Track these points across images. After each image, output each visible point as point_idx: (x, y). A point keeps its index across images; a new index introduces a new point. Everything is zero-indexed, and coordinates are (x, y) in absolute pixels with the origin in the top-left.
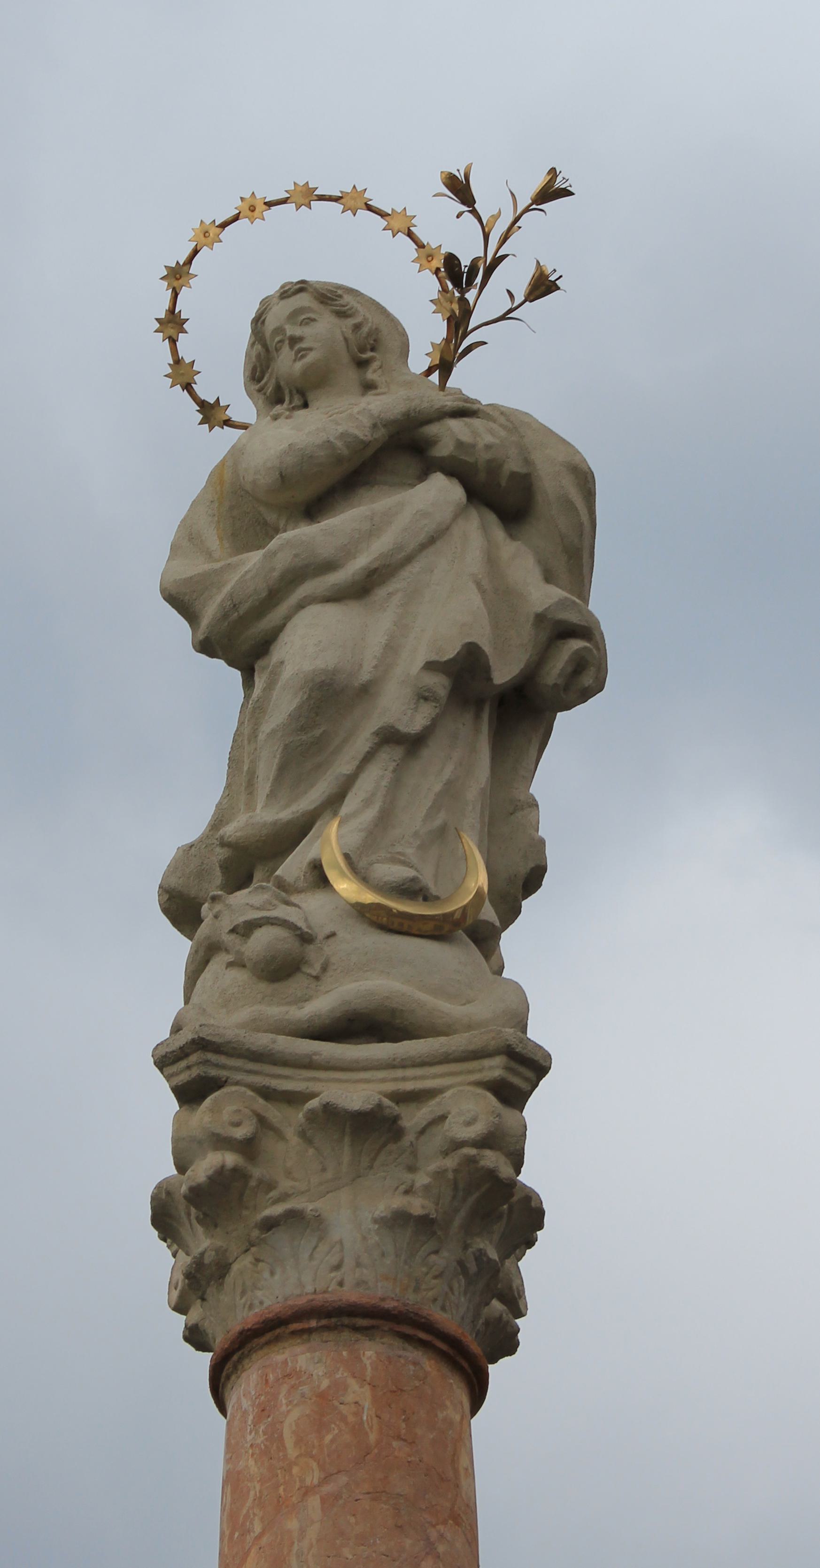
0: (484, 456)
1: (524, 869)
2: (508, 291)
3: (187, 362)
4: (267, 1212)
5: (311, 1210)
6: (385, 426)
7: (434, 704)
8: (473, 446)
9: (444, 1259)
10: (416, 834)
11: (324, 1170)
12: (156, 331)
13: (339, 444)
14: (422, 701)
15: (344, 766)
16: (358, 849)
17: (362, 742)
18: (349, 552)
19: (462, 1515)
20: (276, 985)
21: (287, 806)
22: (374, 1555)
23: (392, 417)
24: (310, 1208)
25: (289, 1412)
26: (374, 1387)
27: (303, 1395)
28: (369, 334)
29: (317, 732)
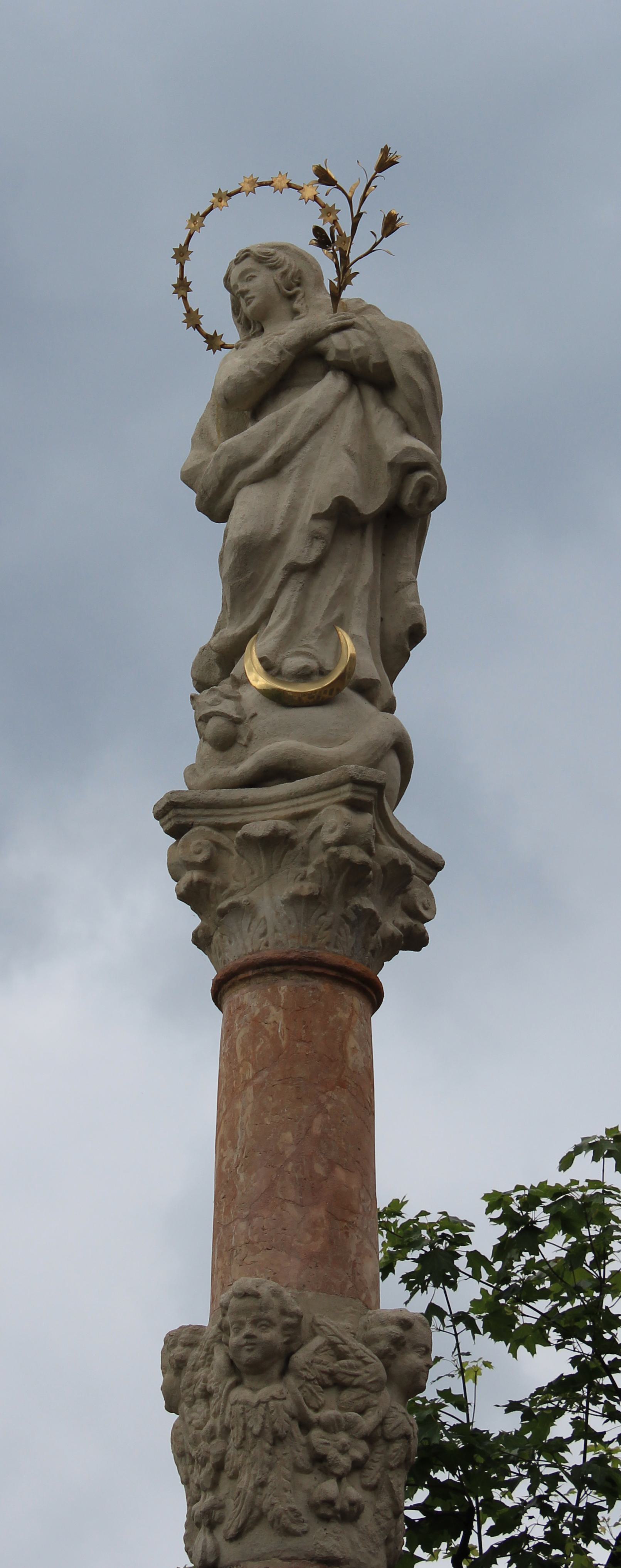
0: (355, 357)
1: (404, 628)
2: (372, 232)
3: (194, 310)
4: (220, 906)
5: (244, 901)
6: (289, 350)
7: (322, 541)
8: (348, 351)
10: (317, 629)
11: (253, 873)
12: (174, 293)
13: (257, 371)
14: (315, 539)
16: (274, 651)
17: (277, 577)
18: (262, 448)
19: (348, 1080)
20: (225, 753)
21: (240, 623)
22: (283, 1120)
23: (294, 343)
24: (244, 900)
25: (239, 1031)
26: (285, 1009)
27: (246, 1021)
28: (293, 277)
29: (248, 575)
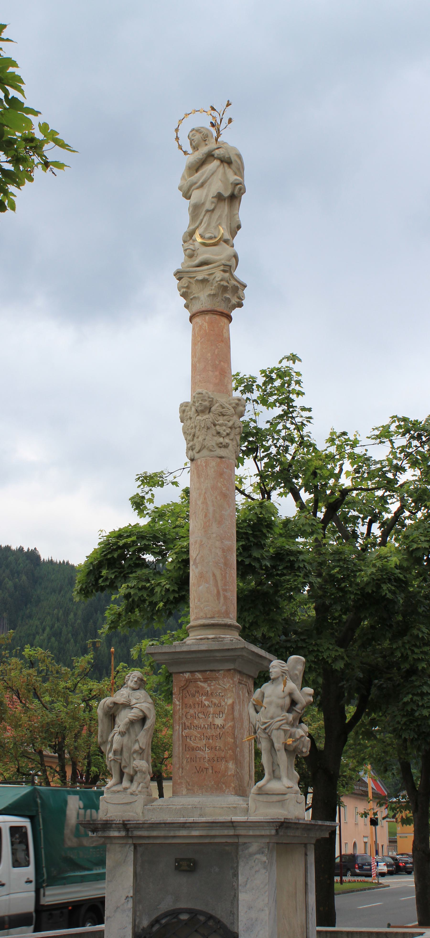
0: (222, 156)
9: (219, 299)
15: (201, 218)
17: (203, 213)
18: (199, 180)
